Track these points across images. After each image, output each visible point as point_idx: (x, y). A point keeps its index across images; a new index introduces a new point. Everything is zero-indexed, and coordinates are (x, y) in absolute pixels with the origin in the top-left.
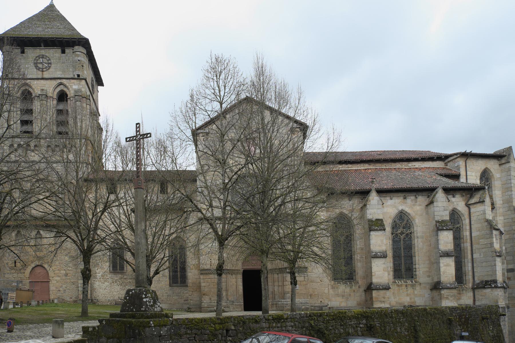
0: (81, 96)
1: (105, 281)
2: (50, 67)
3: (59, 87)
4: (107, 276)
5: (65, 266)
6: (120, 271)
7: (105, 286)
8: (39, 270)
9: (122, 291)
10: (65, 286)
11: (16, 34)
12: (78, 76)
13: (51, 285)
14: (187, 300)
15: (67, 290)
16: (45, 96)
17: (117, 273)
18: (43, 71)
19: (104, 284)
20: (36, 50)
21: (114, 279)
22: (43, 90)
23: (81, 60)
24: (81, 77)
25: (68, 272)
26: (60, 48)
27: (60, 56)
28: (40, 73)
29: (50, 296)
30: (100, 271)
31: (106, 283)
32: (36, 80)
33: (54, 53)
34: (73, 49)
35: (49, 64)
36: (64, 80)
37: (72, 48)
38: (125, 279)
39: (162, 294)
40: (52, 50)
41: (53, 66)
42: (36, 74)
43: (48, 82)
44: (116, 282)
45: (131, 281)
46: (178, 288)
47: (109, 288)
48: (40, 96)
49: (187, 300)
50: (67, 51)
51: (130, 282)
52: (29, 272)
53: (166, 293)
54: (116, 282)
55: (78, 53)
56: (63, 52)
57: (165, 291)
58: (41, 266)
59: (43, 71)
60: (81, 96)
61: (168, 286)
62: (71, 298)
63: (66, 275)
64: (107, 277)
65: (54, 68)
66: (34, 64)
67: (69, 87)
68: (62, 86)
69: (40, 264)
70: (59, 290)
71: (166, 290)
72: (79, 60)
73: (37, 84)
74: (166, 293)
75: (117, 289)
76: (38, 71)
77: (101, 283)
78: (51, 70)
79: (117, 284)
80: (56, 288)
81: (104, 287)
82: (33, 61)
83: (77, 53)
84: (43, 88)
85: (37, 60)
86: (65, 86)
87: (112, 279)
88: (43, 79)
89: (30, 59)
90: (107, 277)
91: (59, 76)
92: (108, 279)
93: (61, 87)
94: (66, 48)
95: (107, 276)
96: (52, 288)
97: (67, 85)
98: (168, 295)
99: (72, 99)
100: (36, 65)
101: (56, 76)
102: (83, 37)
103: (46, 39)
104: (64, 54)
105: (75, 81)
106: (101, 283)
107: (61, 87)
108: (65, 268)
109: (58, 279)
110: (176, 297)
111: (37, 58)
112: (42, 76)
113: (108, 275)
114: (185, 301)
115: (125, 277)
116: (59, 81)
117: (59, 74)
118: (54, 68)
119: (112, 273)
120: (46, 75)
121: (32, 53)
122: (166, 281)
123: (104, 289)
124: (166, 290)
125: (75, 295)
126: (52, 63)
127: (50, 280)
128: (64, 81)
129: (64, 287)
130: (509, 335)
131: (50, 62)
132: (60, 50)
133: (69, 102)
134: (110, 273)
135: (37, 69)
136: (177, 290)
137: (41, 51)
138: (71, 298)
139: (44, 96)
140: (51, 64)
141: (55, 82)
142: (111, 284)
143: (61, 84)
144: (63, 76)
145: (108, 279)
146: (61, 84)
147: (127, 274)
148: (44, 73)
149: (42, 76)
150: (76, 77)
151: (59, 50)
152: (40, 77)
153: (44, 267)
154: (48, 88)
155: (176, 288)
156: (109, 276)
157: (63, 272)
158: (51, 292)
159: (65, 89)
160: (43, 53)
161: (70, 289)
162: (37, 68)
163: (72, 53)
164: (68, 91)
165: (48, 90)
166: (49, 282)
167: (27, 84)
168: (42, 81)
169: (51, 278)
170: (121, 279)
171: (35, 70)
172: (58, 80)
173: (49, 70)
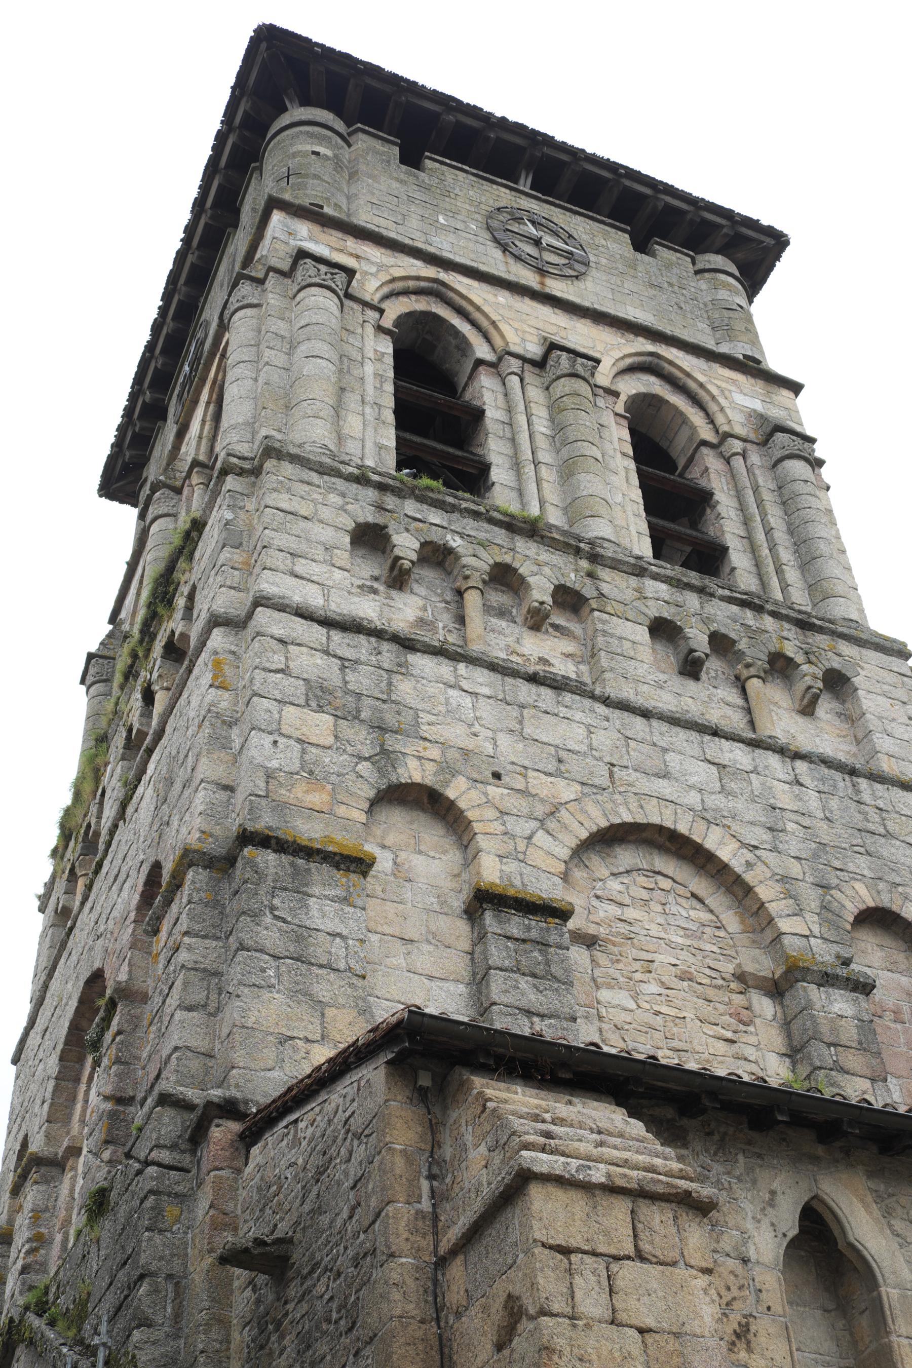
20: (495, 187)
94: (427, 154)
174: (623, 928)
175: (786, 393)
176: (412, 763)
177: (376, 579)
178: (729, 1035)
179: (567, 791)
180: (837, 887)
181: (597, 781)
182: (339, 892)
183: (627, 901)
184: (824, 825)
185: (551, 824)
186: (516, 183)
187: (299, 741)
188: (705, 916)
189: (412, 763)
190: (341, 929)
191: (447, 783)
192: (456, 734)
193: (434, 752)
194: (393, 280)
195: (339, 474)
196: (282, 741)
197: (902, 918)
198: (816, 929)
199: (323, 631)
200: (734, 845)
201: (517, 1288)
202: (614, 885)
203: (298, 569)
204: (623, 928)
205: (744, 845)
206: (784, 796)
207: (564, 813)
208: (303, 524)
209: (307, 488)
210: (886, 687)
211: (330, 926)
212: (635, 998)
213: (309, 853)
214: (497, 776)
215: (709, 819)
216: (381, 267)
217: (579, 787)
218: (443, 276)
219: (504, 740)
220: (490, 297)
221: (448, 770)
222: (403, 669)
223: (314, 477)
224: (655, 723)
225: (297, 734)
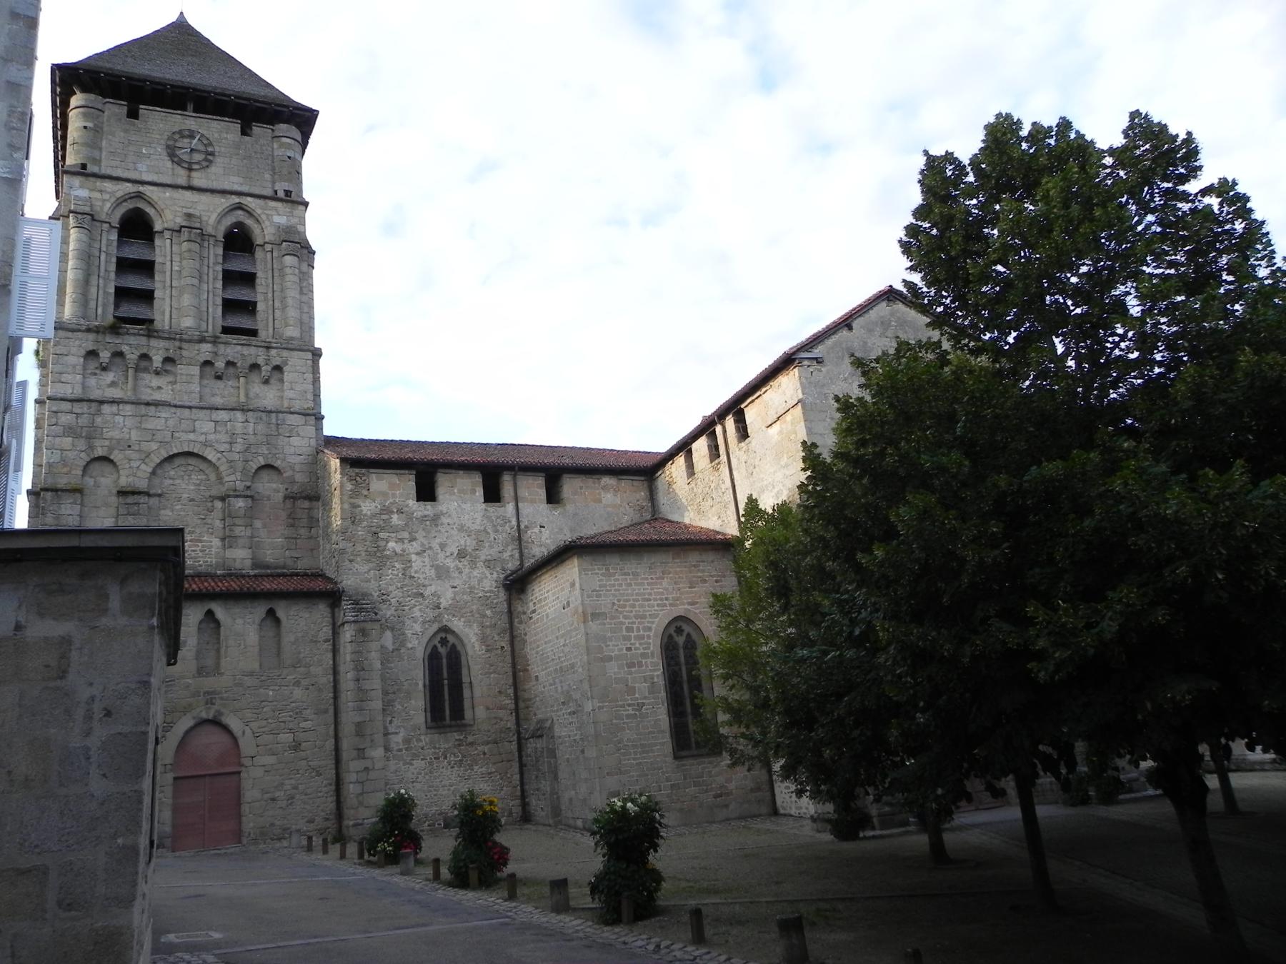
0: (298, 243)
1: (415, 756)
2: (211, 162)
3: (231, 213)
4: (421, 741)
5: (291, 716)
6: (453, 723)
7: (415, 772)
8: (211, 741)
9: (461, 784)
10: (293, 782)
11: (119, 66)
12: (288, 193)
13: (247, 784)
14: (720, 796)
15: (297, 797)
16: (89, 217)
17: (448, 729)
18: (190, 170)
19: (412, 764)
20: (174, 116)
21: (439, 748)
22: (189, 216)
23: (294, 158)
24: (294, 197)
25: (301, 736)
26: (125, 103)
27: (237, 140)
28: (183, 172)
29: (240, 823)
30: (399, 727)
31: (418, 763)
32: (170, 189)
33: (221, 131)
34: (273, 130)
35: (208, 154)
36: (249, 199)
37: (271, 127)
38: (471, 744)
39: (657, 782)
40: (216, 122)
41: (219, 160)
42: (170, 173)
43: (205, 198)
44: (446, 758)
45: (486, 749)
46: (695, 762)
47: (427, 777)
48: (183, 229)
49: (720, 796)
50: (144, 110)
51: (484, 754)
52: (176, 744)
53: (668, 780)
54: (446, 758)
55: (288, 140)
56: (245, 132)
57: (663, 773)
58: (216, 723)
59: (190, 170)
60: (298, 243)
61: (670, 759)
62: (311, 821)
63: (296, 747)
64: (420, 744)
65: (223, 165)
66: (168, 147)
67: (264, 217)
68: (240, 212)
69: (210, 717)
70: (273, 800)
71: (667, 772)
72: (289, 157)
73: (171, 198)
74: (668, 780)
75: (450, 779)
76: (176, 166)
77: (404, 765)
78: (213, 169)
79: (449, 763)
80: (264, 792)
81: (411, 776)
82: (163, 142)
83: (284, 140)
84: (191, 211)
85: (176, 141)
86: (250, 214)
87: (435, 748)
88: (190, 188)
89: (153, 136)
90: (420, 744)
91: (236, 188)
92: (422, 748)
93: (240, 216)
94: (141, 106)
95: (421, 741)
96: (251, 793)
97: (259, 211)
98: (672, 786)
99: (268, 247)
100: (172, 153)
101: (227, 187)
102: (296, 105)
103: (206, 95)
104: (247, 138)
105: (279, 205)
106: (404, 765)
107: (240, 216)
108: (291, 725)
109: (270, 760)
110: (692, 790)
111: (177, 136)
112: (189, 180)
113: (422, 737)
114: (716, 797)
115: (470, 739)
116: (235, 199)
117: (234, 183)
118: (223, 165)
119: (433, 731)
120: (199, 179)
121: (159, 122)
122: (663, 744)
123: (413, 782)
124: (667, 772)
125: (322, 811)
126: (217, 154)
127: (243, 765)
128: (248, 201)
129: (289, 787)
130: (144, 773)
131: (210, 149)
132: (239, 126)
133: (158, 242)
134: (429, 731)
135: (173, 161)
136: (695, 767)
137: (187, 122)
138: (311, 821)
139: (195, 231)
140: (212, 154)
141: (223, 200)
142: (431, 763)
143: (240, 207)
144: (245, 189)
145: (422, 748)
146: (240, 207)
147: (475, 728)
148: (194, 174)
149: (189, 180)
150: (281, 194)
151: (236, 125)
152: (182, 181)
153: (226, 729)
154: (203, 213)
155: (691, 761)
156: (425, 739)
157: (286, 738)
158: (245, 808)
159: (249, 222)
160: (193, 128)
161: (309, 791)
162: (176, 159)
163: (270, 139)
164: (256, 226)
165: (205, 218)
166: (239, 773)
167: (139, 196)
168: (188, 194)
169: (246, 762)
170: (459, 745)
171: (169, 164)
172: (233, 196)
173: (209, 170)
174: (172, 487)
175: (302, 208)
176: (99, 449)
177: (97, 368)
178: (203, 517)
179: (154, 446)
180: (251, 461)
181: (166, 440)
182: (71, 501)
183: (176, 477)
184: (253, 437)
185: (147, 460)
186: (186, 111)
187: (61, 450)
188: (204, 477)
189: (99, 449)
190: (72, 513)
191: (111, 454)
192: (115, 434)
193: (107, 443)
194: (118, 199)
195: (79, 330)
196: (55, 451)
197: (83, 547)
198: (239, 478)
199: (70, 403)
200: (214, 453)
201: (827, 564)
202: (172, 473)
203: (63, 380)
204: (172, 487)
205: (218, 452)
206: (239, 427)
207: (152, 455)
208: (66, 358)
209: (67, 341)
210: (298, 368)
211: (68, 512)
212: (172, 511)
213: (63, 490)
214: (129, 446)
215: (206, 444)
216: (112, 193)
217: (159, 444)
218: (141, 188)
219: (134, 433)
220: (162, 195)
221: (111, 449)
222: (99, 413)
223: (70, 334)
224: (194, 410)
225: (59, 447)
